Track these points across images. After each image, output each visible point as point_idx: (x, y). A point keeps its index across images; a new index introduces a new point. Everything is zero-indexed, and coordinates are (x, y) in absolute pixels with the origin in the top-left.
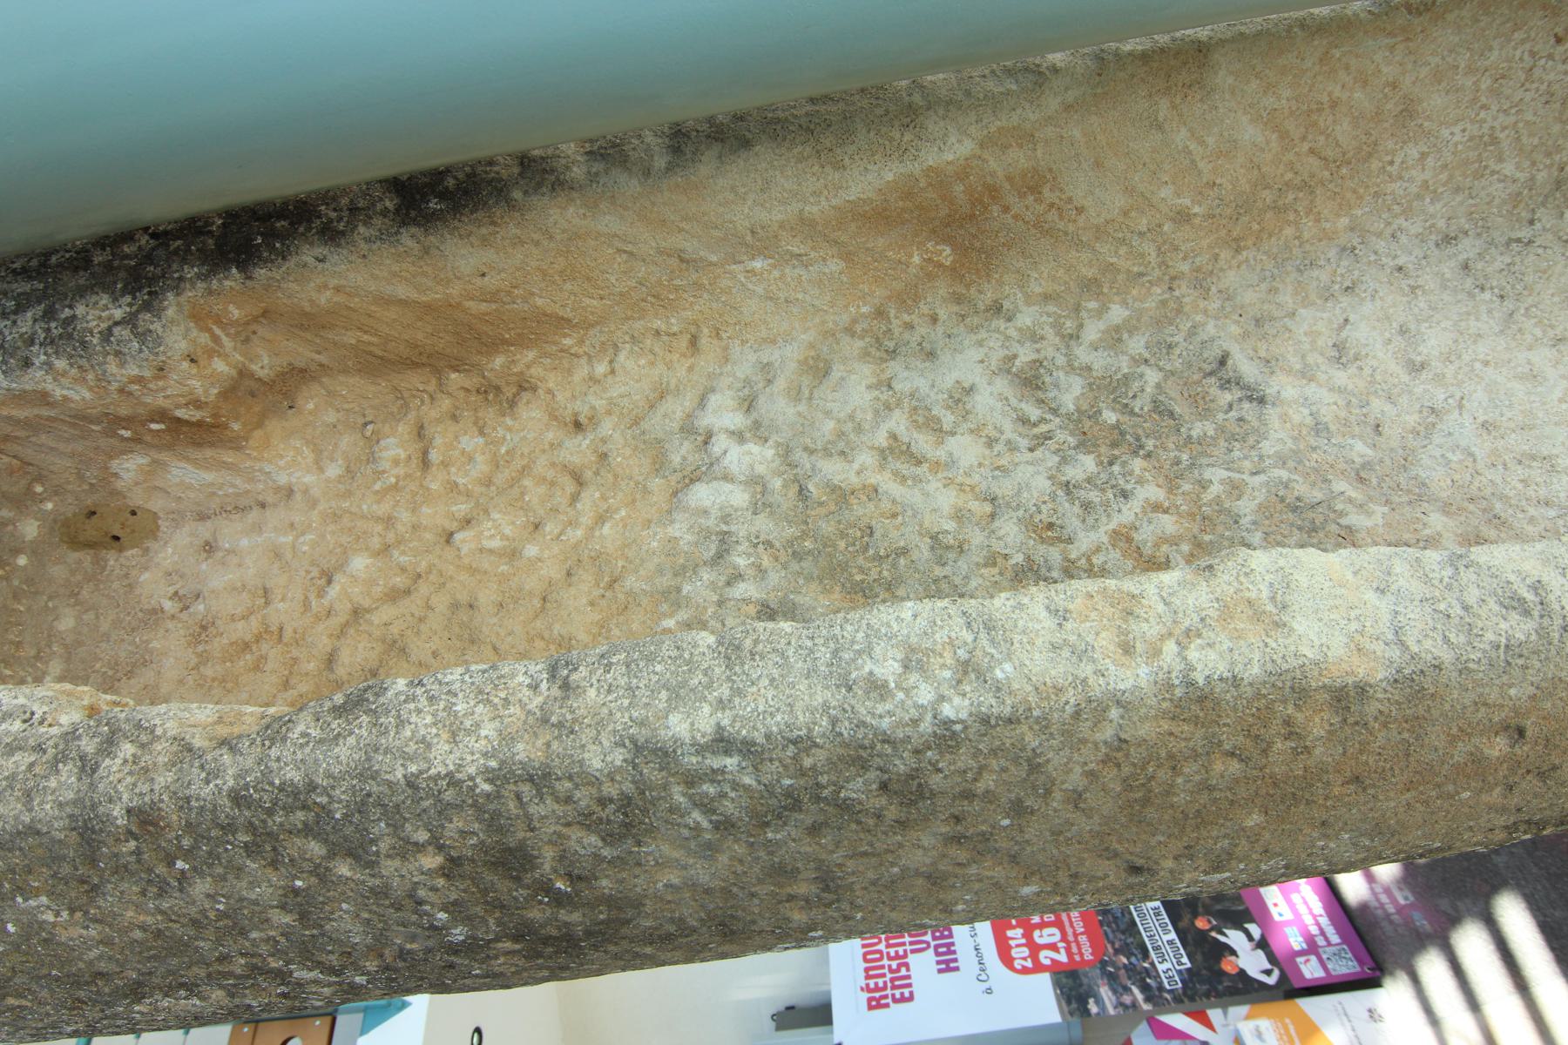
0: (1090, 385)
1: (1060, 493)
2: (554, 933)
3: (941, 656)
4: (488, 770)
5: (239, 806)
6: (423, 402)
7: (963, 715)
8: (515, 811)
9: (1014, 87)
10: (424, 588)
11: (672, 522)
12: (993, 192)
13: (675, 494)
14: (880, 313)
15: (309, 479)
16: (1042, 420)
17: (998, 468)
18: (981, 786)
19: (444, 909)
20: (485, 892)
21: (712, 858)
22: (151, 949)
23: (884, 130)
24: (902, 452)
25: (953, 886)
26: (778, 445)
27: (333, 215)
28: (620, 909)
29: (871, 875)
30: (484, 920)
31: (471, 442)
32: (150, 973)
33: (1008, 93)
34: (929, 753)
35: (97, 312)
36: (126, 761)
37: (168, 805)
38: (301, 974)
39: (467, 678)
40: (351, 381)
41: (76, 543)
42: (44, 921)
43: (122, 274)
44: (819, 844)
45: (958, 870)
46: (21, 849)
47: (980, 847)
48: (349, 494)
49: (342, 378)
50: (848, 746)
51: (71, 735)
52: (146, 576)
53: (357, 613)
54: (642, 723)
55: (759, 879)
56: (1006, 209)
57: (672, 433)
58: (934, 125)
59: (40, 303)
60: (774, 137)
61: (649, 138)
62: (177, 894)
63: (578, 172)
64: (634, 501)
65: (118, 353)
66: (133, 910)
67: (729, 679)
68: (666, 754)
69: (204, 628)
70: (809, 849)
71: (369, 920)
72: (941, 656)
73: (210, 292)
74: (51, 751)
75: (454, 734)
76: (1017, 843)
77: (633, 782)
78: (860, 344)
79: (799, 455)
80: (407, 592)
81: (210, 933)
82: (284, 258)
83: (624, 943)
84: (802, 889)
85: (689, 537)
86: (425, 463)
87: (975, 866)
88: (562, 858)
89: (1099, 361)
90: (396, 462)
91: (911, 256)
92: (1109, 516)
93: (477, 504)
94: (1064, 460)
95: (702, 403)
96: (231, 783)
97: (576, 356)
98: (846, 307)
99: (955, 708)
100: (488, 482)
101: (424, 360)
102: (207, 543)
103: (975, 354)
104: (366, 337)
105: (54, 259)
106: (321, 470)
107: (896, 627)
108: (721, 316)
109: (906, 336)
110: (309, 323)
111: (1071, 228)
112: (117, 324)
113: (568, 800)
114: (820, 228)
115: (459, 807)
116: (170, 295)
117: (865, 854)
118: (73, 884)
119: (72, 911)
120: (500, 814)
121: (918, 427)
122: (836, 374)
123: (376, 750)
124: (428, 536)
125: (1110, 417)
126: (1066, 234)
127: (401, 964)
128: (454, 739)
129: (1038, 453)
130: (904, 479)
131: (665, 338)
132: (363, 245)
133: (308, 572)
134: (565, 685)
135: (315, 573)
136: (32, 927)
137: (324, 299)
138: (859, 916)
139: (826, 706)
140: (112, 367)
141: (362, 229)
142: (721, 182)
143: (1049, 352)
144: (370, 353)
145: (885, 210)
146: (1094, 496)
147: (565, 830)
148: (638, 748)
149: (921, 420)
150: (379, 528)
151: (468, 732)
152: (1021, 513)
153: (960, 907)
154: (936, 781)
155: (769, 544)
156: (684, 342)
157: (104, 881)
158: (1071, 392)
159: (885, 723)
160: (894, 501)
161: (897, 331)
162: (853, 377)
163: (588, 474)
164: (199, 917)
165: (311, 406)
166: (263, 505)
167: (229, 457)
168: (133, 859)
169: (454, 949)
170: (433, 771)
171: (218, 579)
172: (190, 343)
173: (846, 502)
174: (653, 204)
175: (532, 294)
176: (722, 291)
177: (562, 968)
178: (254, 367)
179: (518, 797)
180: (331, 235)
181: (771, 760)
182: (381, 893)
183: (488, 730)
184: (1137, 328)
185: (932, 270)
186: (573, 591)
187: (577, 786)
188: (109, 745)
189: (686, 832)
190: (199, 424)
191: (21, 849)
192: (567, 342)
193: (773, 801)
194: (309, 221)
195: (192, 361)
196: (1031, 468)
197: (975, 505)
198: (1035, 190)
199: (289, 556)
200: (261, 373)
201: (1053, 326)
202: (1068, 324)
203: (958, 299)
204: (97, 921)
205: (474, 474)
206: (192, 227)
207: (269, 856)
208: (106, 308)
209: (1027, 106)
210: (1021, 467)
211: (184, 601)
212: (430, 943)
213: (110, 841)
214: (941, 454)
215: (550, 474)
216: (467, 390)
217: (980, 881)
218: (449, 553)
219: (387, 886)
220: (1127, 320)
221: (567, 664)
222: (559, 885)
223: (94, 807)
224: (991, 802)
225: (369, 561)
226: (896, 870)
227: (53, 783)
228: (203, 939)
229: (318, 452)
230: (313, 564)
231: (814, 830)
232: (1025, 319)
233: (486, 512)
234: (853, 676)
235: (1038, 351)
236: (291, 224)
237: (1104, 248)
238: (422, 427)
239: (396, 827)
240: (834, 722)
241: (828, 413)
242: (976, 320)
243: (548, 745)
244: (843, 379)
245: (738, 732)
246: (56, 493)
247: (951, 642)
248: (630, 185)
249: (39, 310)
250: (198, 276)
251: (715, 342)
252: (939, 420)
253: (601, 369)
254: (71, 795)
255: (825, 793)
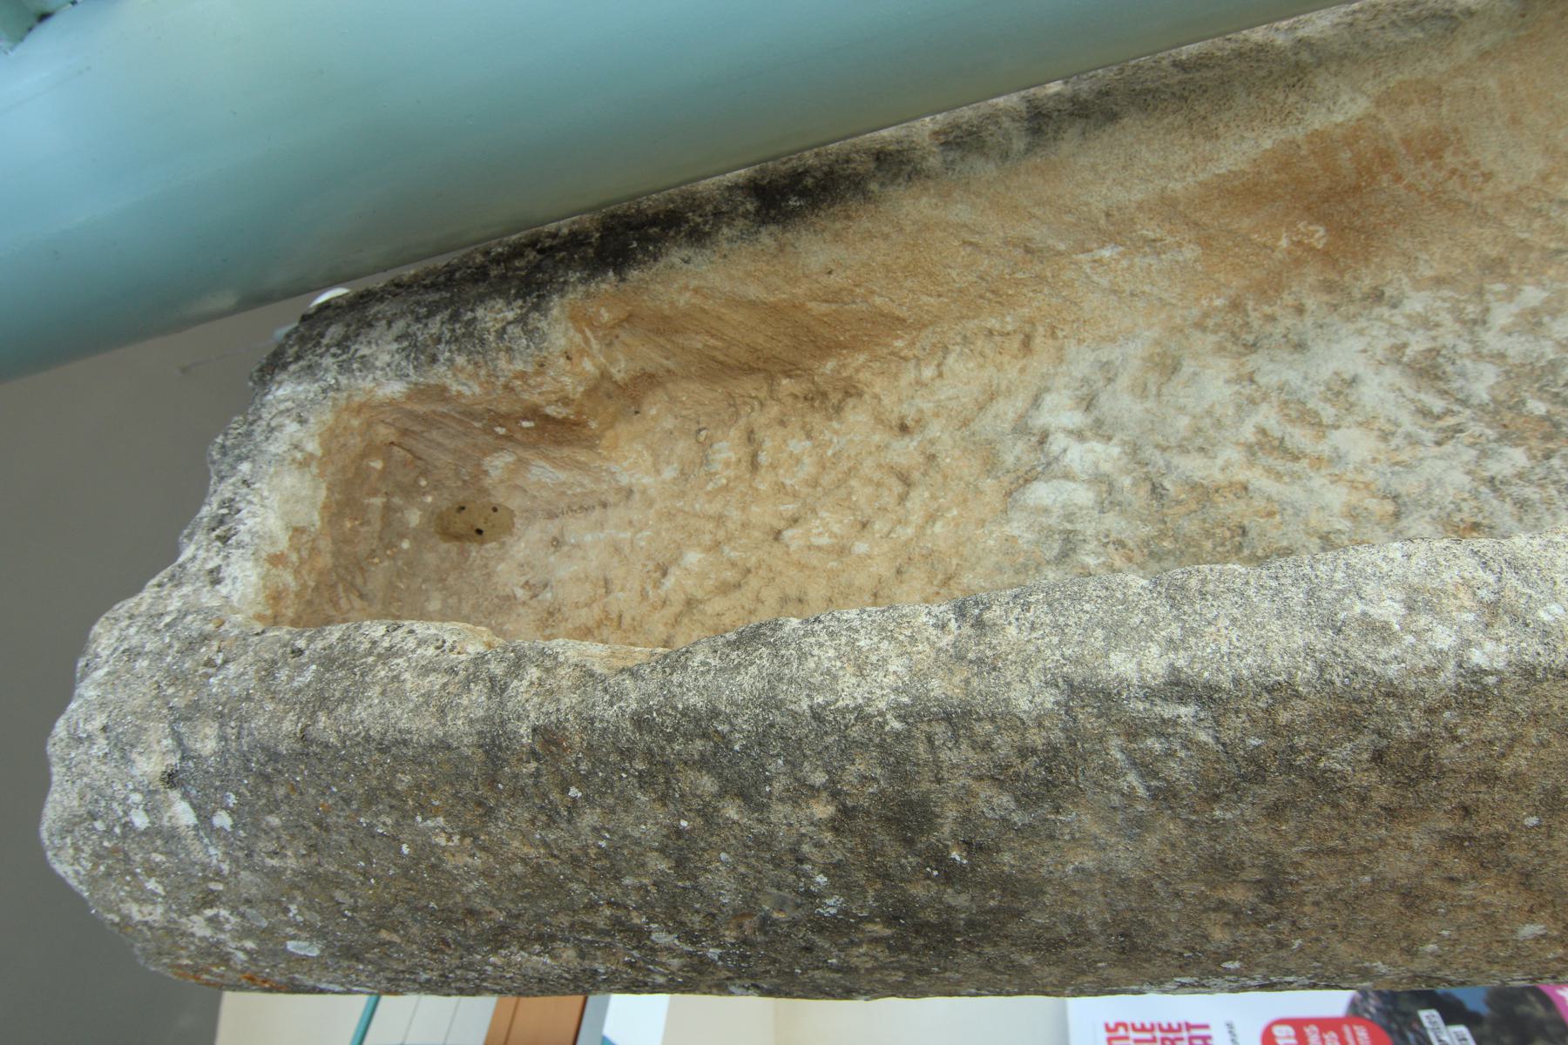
0: (1507, 372)
1: (1483, 489)
2: (933, 918)
3: (1456, 597)
4: (899, 706)
5: (640, 729)
6: (753, 409)
7: (1500, 664)
8: (924, 756)
9: (1420, 35)
10: (754, 582)
11: (1009, 521)
12: (1385, 158)
13: (1009, 494)
14: (1236, 306)
15: (647, 480)
16: (1448, 412)
17: (1397, 463)
18: (1508, 766)
19: (824, 872)
20: (872, 854)
21: (1139, 839)
22: (525, 886)
23: (1266, 92)
24: (1274, 448)
25: (1434, 913)
26: (1124, 443)
27: (699, 220)
28: (1015, 895)
29: (1333, 883)
30: (864, 891)
31: (798, 445)
32: (518, 916)
33: (1414, 42)
34: (1447, 714)
35: (494, 315)
36: (532, 683)
37: (572, 725)
38: (661, 938)
39: (865, 616)
40: (692, 387)
41: (448, 534)
42: (437, 845)
43: (516, 282)
44: (1276, 831)
45: (1448, 889)
46: (430, 764)
47: (1488, 855)
48: (683, 494)
49: (684, 384)
50: (1339, 698)
51: (480, 660)
52: (501, 567)
53: (690, 603)
54: (1078, 662)
55: (1190, 873)
56: (1398, 178)
57: (1003, 434)
58: (1323, 83)
59: (447, 308)
60: (1144, 108)
61: (1006, 123)
62: (564, 825)
63: (934, 162)
64: (965, 501)
65: (509, 350)
66: (518, 838)
67: (1177, 618)
68: (1108, 696)
69: (551, 614)
70: (1263, 837)
71: (744, 876)
72: (1456, 597)
73: (588, 295)
74: (462, 674)
75: (860, 668)
76: (1539, 853)
77: (1064, 730)
78: (1212, 338)
79: (1149, 452)
80: (738, 586)
81: (585, 874)
82: (656, 260)
83: (1005, 944)
84: (1238, 895)
85: (1028, 536)
86: (754, 465)
87: (1472, 884)
88: (964, 820)
89: (1516, 347)
90: (727, 465)
91: (1278, 239)
92: (1554, 514)
93: (804, 504)
94: (1484, 454)
95: (1036, 402)
96: (634, 706)
97: (905, 359)
98: (1197, 300)
99: (1488, 654)
100: (814, 483)
101: (761, 365)
102: (555, 539)
103: (1358, 343)
104: (712, 342)
105: (457, 275)
106: (658, 472)
107: (1386, 568)
108: (1059, 312)
109: (1268, 328)
110: (665, 326)
111: (1475, 197)
112: (509, 323)
113: (986, 746)
114: (1181, 208)
115: (863, 746)
116: (555, 298)
117: (1333, 851)
118: (471, 805)
119: (464, 835)
120: (907, 759)
121: (1292, 421)
122: (1188, 367)
123: (780, 680)
124: (756, 534)
125: (1538, 407)
126: (1468, 205)
127: (760, 938)
128: (860, 672)
129: (1448, 447)
130: (1279, 476)
131: (998, 338)
132: (725, 245)
133: (644, 566)
134: (979, 624)
135: (651, 566)
136: (425, 850)
137: (683, 300)
138: (1297, 943)
139: (1309, 651)
140: (502, 363)
141: (725, 230)
142: (1082, 161)
143: (1449, 340)
144: (713, 359)
145: (1256, 185)
146: (1530, 492)
147: (975, 786)
148: (1073, 688)
149: (1294, 414)
150: (711, 526)
151: (876, 667)
152: (1434, 511)
153: (1430, 947)
154: (1449, 753)
155: (1120, 544)
156: (1016, 343)
157: (500, 804)
158: (1484, 383)
159: (1393, 670)
160: (1269, 499)
161: (1256, 324)
162: (1209, 371)
163: (916, 475)
164: (579, 853)
165: (653, 412)
166: (604, 505)
167: (582, 456)
168: (530, 781)
169: (820, 925)
170: (840, 704)
171: (564, 569)
172: (567, 343)
173: (1209, 500)
174: (1008, 188)
175: (873, 292)
176: (1065, 285)
177: (923, 972)
178: (613, 370)
179: (930, 739)
180: (698, 237)
181: (1237, 712)
182: (763, 843)
183: (896, 665)
184: (1560, 311)
185: (1302, 254)
186: (905, 587)
187: (998, 730)
188: (517, 667)
189: (1116, 799)
190: (563, 422)
191: (430, 764)
192: (899, 344)
193: (1232, 767)
194: (679, 225)
195: (568, 358)
196: (1441, 464)
197: (1372, 503)
198: (1435, 154)
199: (627, 550)
200: (618, 377)
201: (1451, 311)
202: (1470, 308)
203: (1329, 287)
204: (484, 849)
205: (802, 475)
206: (575, 240)
207: (661, 788)
208: (501, 311)
209: (1435, 54)
210: (1426, 464)
211: (534, 589)
212: (798, 914)
213: (513, 761)
214: (1324, 448)
215: (877, 476)
216: (796, 397)
217: (1471, 908)
218: (778, 549)
219: (772, 835)
220: (1547, 302)
221: (977, 603)
222: (955, 855)
223: (503, 723)
224: (1517, 790)
225: (701, 556)
226: (1367, 878)
227: (465, 701)
228: (577, 880)
229: (656, 457)
230: (649, 558)
231: (1275, 811)
232: (1416, 303)
233: (814, 511)
234: (1342, 616)
235: (1434, 339)
236: (663, 229)
237: (1514, 222)
238: (752, 432)
239: (793, 765)
240: (1322, 667)
241: (1182, 409)
242: (1352, 309)
243: (967, 682)
244: (1195, 374)
245: (1199, 674)
246: (436, 488)
247: (1466, 583)
248: (985, 169)
249: (446, 314)
250: (580, 280)
251: (1050, 342)
252: (1316, 414)
253: (928, 372)
254: (481, 713)
255: (1300, 760)
